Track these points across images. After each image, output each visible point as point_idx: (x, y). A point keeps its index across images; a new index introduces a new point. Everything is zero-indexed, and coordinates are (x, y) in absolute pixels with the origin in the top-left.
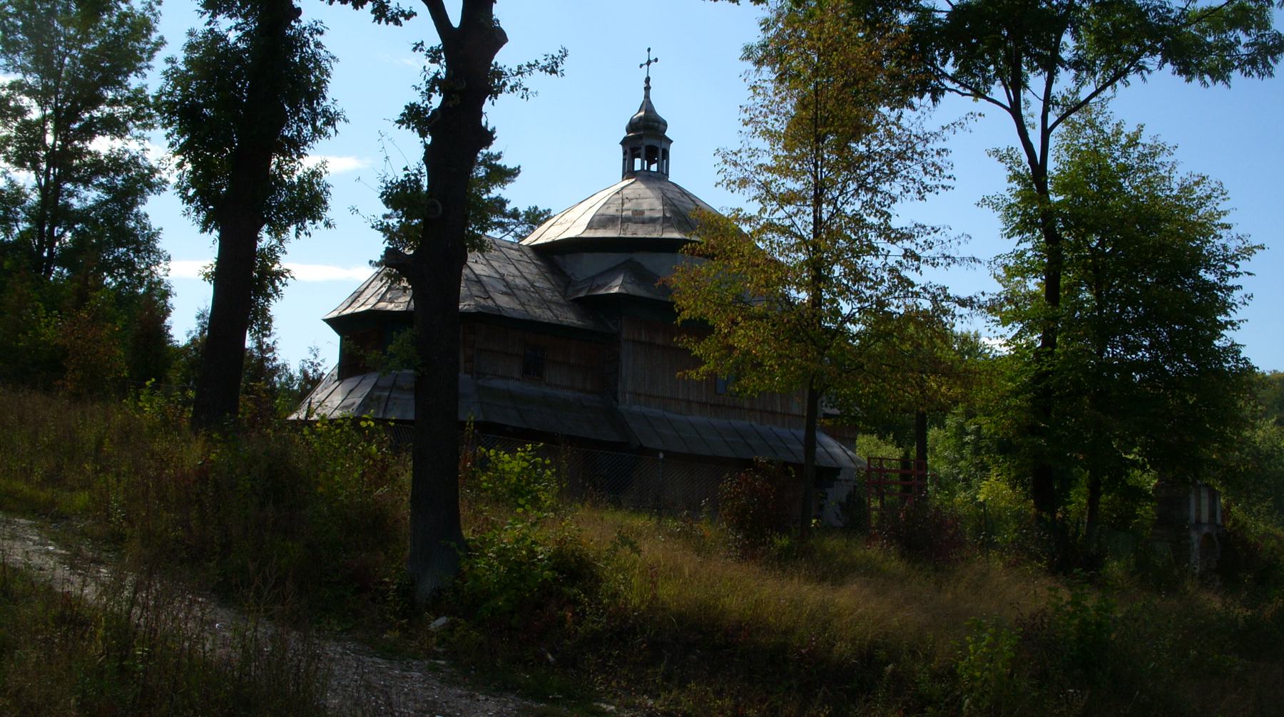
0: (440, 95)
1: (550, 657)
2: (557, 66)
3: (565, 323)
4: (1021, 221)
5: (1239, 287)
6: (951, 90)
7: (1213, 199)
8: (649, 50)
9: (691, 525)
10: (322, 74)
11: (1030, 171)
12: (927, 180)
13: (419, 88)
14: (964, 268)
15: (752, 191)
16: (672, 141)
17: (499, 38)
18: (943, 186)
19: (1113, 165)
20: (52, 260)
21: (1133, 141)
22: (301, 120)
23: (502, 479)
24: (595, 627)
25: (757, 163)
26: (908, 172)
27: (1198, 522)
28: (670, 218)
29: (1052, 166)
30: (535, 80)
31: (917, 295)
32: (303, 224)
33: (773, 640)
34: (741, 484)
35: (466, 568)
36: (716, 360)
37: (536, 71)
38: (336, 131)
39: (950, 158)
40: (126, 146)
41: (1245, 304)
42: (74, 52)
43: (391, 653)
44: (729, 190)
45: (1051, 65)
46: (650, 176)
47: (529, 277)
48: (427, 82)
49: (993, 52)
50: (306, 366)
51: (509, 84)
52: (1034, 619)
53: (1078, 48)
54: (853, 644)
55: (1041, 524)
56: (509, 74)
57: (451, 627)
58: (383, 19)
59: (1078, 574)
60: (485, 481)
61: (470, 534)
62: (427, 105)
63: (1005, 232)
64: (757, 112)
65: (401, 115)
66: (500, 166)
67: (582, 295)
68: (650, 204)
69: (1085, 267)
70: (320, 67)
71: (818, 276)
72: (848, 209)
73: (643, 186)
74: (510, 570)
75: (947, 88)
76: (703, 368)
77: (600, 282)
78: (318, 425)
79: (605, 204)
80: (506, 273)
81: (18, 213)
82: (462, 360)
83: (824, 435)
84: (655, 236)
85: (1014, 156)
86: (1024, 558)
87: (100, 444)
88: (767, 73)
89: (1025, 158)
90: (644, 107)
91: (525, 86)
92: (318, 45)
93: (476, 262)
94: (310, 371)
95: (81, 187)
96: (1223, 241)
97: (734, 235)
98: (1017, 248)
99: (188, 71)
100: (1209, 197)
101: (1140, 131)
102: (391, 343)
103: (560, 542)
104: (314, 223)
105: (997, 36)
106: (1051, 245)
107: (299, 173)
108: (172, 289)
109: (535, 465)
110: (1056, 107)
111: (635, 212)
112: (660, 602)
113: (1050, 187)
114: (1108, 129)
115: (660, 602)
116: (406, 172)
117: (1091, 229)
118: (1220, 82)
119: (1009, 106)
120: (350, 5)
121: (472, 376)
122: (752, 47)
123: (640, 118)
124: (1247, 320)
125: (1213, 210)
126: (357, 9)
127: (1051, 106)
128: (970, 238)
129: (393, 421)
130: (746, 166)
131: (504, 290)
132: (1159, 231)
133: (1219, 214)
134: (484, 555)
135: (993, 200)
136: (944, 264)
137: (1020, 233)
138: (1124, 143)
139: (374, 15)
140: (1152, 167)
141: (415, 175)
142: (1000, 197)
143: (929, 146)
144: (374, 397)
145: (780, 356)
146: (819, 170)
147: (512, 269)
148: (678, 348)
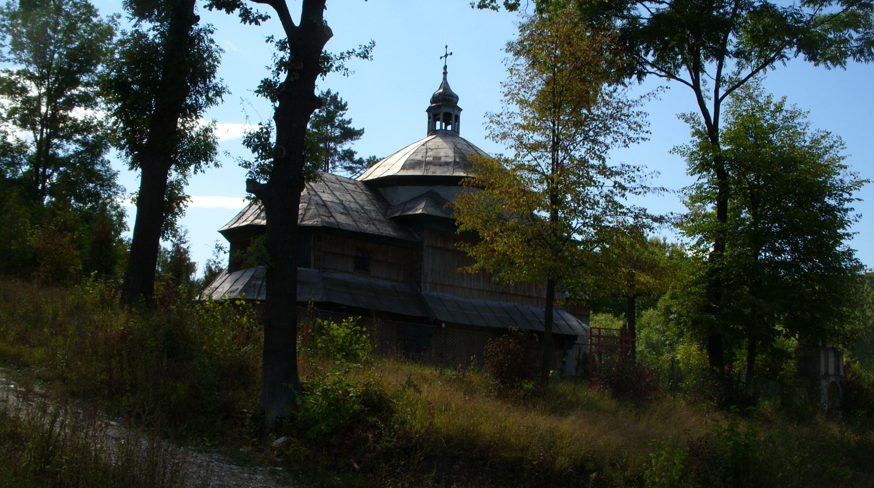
0: (285, 73)
1: (356, 465)
2: (368, 53)
3: (384, 234)
4: (701, 163)
5: (852, 209)
6: (651, 73)
7: (834, 148)
8: (446, 47)
9: (464, 374)
10: (214, 61)
11: (706, 129)
12: (631, 134)
13: (270, 68)
14: (656, 194)
15: (510, 142)
16: (462, 110)
17: (326, 34)
18: (642, 139)
19: (765, 125)
20: (44, 192)
21: (779, 108)
22: (198, 92)
23: (332, 340)
24: (388, 444)
25: (513, 122)
26: (618, 129)
27: (827, 374)
28: (459, 162)
29: (722, 125)
30: (353, 63)
31: (625, 214)
32: (199, 165)
33: (513, 455)
34: (500, 346)
35: (299, 403)
36: (485, 260)
37: (353, 57)
38: (223, 100)
39: (648, 119)
40: (95, 115)
41: (856, 221)
42: (61, 50)
43: (243, 462)
44: (495, 141)
45: (720, 54)
46: (446, 133)
47: (361, 202)
48: (277, 64)
49: (680, 45)
50: (210, 264)
51: (335, 66)
52: (701, 441)
53: (739, 43)
54: (570, 458)
55: (714, 375)
56: (334, 58)
57: (287, 444)
58: (248, 21)
59: (732, 409)
60: (320, 342)
61: (305, 379)
62: (276, 80)
63: (689, 171)
64: (513, 87)
65: (258, 87)
66: (350, 128)
67: (397, 215)
68: (446, 153)
69: (745, 196)
70: (211, 56)
71: (556, 202)
72: (577, 155)
73: (441, 140)
74: (330, 404)
75: (648, 72)
76: (476, 265)
77: (409, 206)
78: (207, 303)
79: (414, 152)
80: (344, 199)
81: (21, 159)
82: (312, 260)
83: (566, 312)
84: (448, 174)
85: (696, 119)
86: (702, 398)
87: (56, 315)
88: (522, 60)
89: (703, 120)
90: (443, 86)
91: (346, 67)
92: (212, 41)
93: (324, 192)
94: (213, 267)
95: (65, 142)
96: (840, 177)
97: (498, 172)
98: (698, 182)
99: (121, 58)
100: (832, 147)
101: (784, 101)
102: (250, 246)
103: (366, 385)
104: (207, 164)
105: (683, 34)
106: (720, 180)
107: (196, 129)
108: (126, 212)
109: (355, 332)
110: (724, 85)
111: (435, 158)
112: (435, 428)
113: (720, 140)
114: (762, 100)
115: (435, 428)
116: (261, 126)
117: (749, 169)
118: (838, 66)
119: (692, 84)
120: (224, 10)
121: (319, 270)
122: (513, 43)
123: (440, 94)
124: (859, 233)
125: (835, 156)
126: (229, 13)
127: (721, 83)
128: (660, 174)
129: (259, 301)
130: (506, 125)
131: (342, 211)
132: (797, 170)
133: (839, 159)
134: (313, 394)
135: (681, 149)
136: (643, 193)
137: (699, 172)
138: (773, 109)
139: (241, 18)
140: (792, 126)
141: (267, 128)
142: (686, 147)
143: (631, 109)
144: (251, 285)
145: (526, 256)
146: (556, 127)
147: (349, 197)
148: (458, 251)
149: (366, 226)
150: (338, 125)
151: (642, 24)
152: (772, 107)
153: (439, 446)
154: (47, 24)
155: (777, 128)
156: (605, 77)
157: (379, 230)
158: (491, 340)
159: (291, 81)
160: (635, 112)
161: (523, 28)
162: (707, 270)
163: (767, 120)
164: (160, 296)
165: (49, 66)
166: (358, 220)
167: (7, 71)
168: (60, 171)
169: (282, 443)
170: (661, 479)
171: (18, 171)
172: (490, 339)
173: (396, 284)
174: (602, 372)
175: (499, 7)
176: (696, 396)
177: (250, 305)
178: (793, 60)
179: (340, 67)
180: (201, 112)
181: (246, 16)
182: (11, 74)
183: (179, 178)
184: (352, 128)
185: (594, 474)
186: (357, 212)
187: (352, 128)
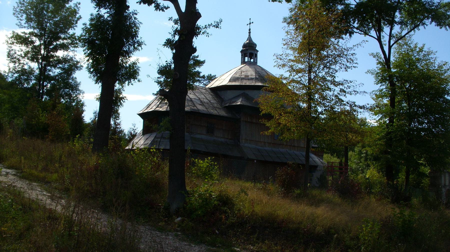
1: (217, 231)
3: (221, 115)
6: (356, 32)
8: (250, 19)
11: (384, 61)
12: (348, 64)
13: (171, 33)
14: (361, 95)
15: (287, 68)
16: (258, 51)
17: (198, 16)
18: (354, 67)
19: (414, 58)
20: (43, 94)
21: (421, 50)
22: (130, 44)
25: (288, 59)
26: (341, 62)
28: (258, 78)
29: (392, 59)
30: (211, 30)
31: (345, 105)
32: (130, 81)
33: (294, 226)
34: (283, 171)
35: (188, 200)
36: (274, 128)
37: (211, 27)
38: (142, 48)
39: (356, 56)
43: (161, 230)
44: (279, 68)
45: (392, 23)
46: (251, 63)
47: (209, 99)
48: (174, 31)
49: (371, 19)
51: (202, 32)
53: (401, 17)
54: (323, 227)
56: (202, 28)
57: (182, 221)
58: (158, 9)
60: (194, 170)
61: (189, 188)
63: (376, 82)
64: (288, 41)
66: (198, 60)
67: (227, 105)
68: (251, 73)
70: (136, 26)
71: (310, 98)
73: (248, 67)
74: (203, 201)
75: (355, 32)
77: (233, 100)
78: (136, 151)
80: (201, 97)
84: (253, 84)
85: (379, 56)
87: (61, 157)
88: (292, 27)
90: (249, 39)
91: (207, 32)
92: (135, 18)
93: (190, 94)
94: (133, 132)
98: (380, 88)
99: (91, 28)
102: (162, 122)
104: (134, 80)
109: (211, 164)
111: (246, 76)
113: (391, 66)
114: (412, 46)
116: (167, 63)
117: (406, 81)
119: (377, 38)
120: (147, 4)
122: (286, 18)
123: (247, 43)
126: (149, 6)
128: (363, 85)
130: (284, 60)
131: (200, 103)
134: (194, 196)
135: (371, 71)
137: (381, 83)
138: (418, 51)
139: (155, 8)
140: (428, 59)
141: (170, 64)
142: (374, 70)
143: (349, 52)
145: (297, 126)
146: (310, 61)
147: (203, 96)
149: (212, 111)
150: (192, 58)
151: (352, 8)
152: (417, 49)
153: (258, 221)
154: (43, 8)
155: (420, 60)
156: (333, 35)
157: (219, 113)
158: (279, 169)
159: (181, 40)
160: (351, 53)
161: (291, 10)
162: (385, 133)
163: (415, 56)
164: (111, 147)
165: (44, 30)
166: (208, 108)
167: (24, 33)
168: (52, 83)
169: (180, 220)
170: (368, 238)
171: (30, 83)
172: (278, 168)
173: (227, 140)
174: (334, 184)
175: (282, 1)
176: (381, 196)
177: (158, 151)
178: (429, 25)
179: (204, 32)
180: (131, 54)
181: (158, 7)
182: (26, 34)
183: (120, 87)
184: (199, 60)
185: (335, 235)
186: (207, 104)
187: (199, 60)
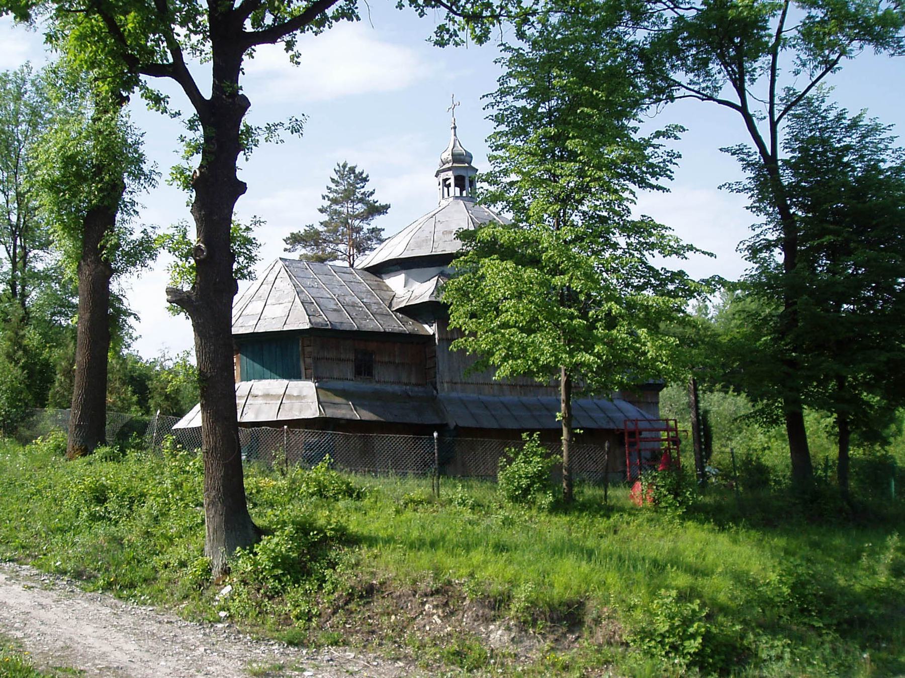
17: (244, 104)
21: (854, 124)
29: (783, 155)
89: (755, 148)
